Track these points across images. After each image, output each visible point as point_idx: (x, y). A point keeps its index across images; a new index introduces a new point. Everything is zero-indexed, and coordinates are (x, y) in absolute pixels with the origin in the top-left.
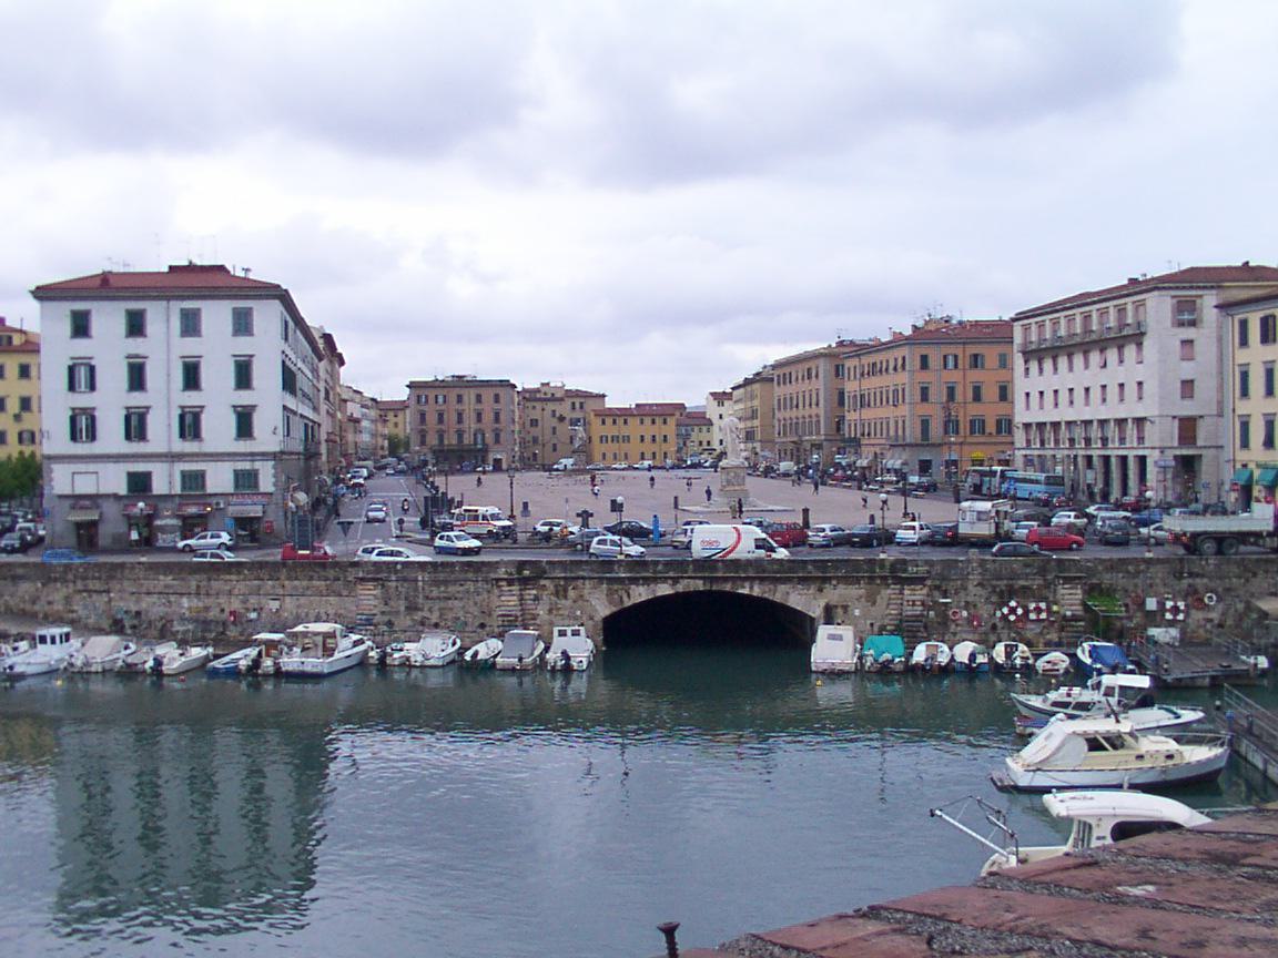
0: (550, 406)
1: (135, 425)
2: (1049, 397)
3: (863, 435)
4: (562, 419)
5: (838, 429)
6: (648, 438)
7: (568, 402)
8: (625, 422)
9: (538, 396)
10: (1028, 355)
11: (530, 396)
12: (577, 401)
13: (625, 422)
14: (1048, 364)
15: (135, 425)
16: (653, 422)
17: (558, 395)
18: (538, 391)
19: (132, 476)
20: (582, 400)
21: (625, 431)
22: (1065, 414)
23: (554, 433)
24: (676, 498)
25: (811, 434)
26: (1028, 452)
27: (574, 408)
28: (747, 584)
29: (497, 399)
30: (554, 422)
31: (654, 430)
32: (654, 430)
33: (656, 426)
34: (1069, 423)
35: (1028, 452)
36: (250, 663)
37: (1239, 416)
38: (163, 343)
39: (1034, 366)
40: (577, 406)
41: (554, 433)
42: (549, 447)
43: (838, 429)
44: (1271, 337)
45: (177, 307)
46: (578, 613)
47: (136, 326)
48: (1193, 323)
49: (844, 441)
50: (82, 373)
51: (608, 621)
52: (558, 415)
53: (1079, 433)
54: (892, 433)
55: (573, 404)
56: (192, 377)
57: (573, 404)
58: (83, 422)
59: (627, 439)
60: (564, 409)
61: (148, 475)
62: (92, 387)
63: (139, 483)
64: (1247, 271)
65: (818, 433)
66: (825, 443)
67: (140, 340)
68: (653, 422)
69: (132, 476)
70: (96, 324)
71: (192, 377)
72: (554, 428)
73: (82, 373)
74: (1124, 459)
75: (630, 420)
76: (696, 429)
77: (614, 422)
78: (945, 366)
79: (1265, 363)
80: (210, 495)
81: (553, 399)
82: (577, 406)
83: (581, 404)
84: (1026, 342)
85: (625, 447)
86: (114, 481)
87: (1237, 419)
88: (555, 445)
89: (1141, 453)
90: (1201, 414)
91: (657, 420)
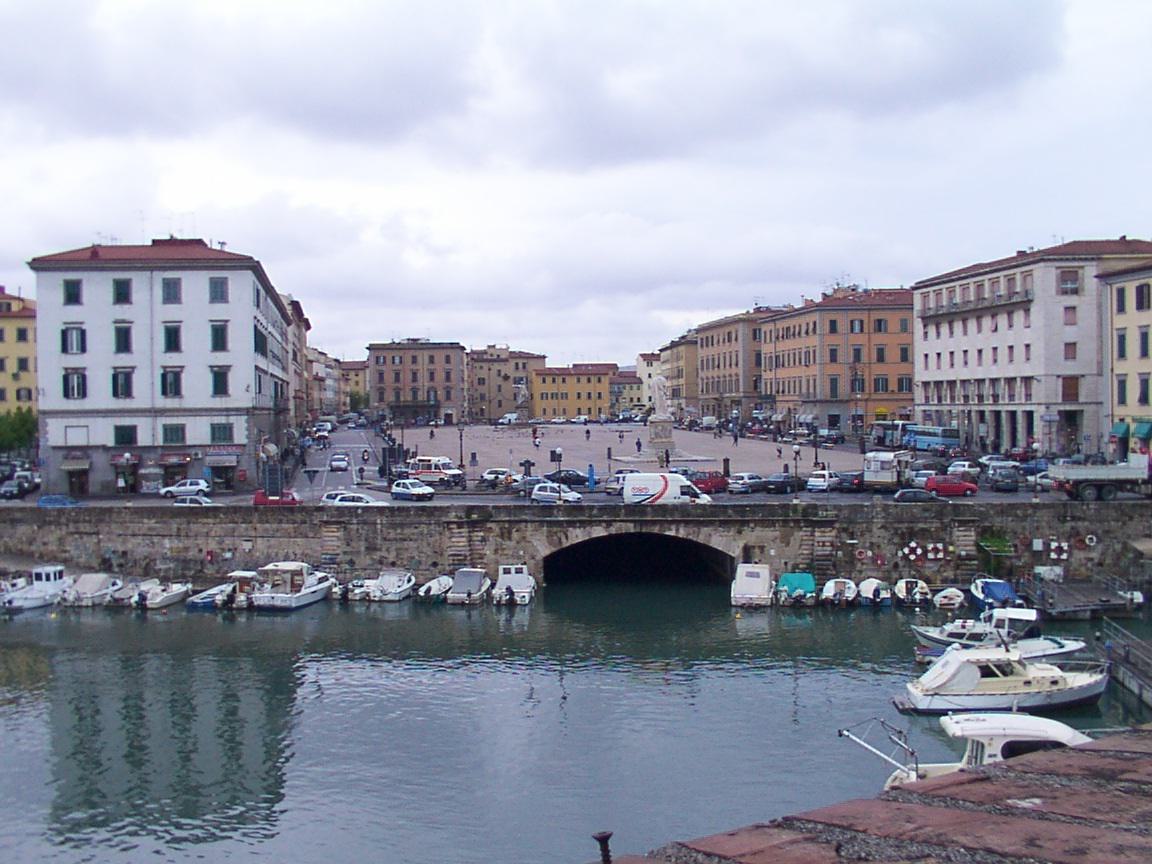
0: (496, 367)
1: (122, 384)
2: (945, 358)
3: (778, 392)
4: (506, 378)
5: (756, 387)
6: (584, 396)
7: (512, 363)
8: (564, 381)
9: (485, 357)
10: (927, 320)
11: (478, 357)
12: (521, 362)
13: (564, 381)
14: (945, 329)
15: (122, 384)
16: (589, 381)
17: (503, 356)
18: (485, 352)
19: (119, 430)
20: (525, 361)
21: (564, 389)
22: (960, 373)
23: (500, 390)
24: (609, 449)
25: (731, 391)
26: (927, 408)
27: (517, 368)
28: (673, 527)
29: (448, 360)
30: (500, 381)
31: (589, 388)
32: (589, 388)
33: (591, 385)
34: (963, 382)
35: (927, 408)
36: (225, 598)
37: (1118, 375)
38: (147, 309)
39: (932, 330)
40: (521, 366)
41: (500, 390)
42: (495, 403)
43: (756, 387)
44: (1146, 304)
45: (159, 277)
46: (521, 553)
47: (122, 294)
48: (1075, 292)
49: (760, 397)
50: (74, 337)
51: (548, 560)
52: (503, 374)
53: (972, 390)
54: (804, 390)
55: (517, 364)
56: (173, 340)
57: (517, 364)
58: (75, 380)
59: (565, 396)
60: (508, 369)
61: (133, 429)
62: (83, 349)
63: (126, 436)
64: (1124, 245)
65: (738, 391)
66: (743, 400)
67: (126, 306)
68: (589, 381)
69: (119, 430)
70: (87, 293)
71: (173, 340)
72: (500, 386)
73: (74, 337)
74: (1013, 414)
75: (568, 379)
76: (628, 387)
77: (554, 381)
78: (852, 330)
79: (1140, 327)
80: (190, 446)
81: (499, 360)
82: (521, 366)
83: (524, 364)
84: (925, 308)
85: (564, 403)
86: (103, 433)
87: (1115, 378)
88: (500, 402)
89: (1028, 408)
90: (1083, 373)
91: (593, 378)
